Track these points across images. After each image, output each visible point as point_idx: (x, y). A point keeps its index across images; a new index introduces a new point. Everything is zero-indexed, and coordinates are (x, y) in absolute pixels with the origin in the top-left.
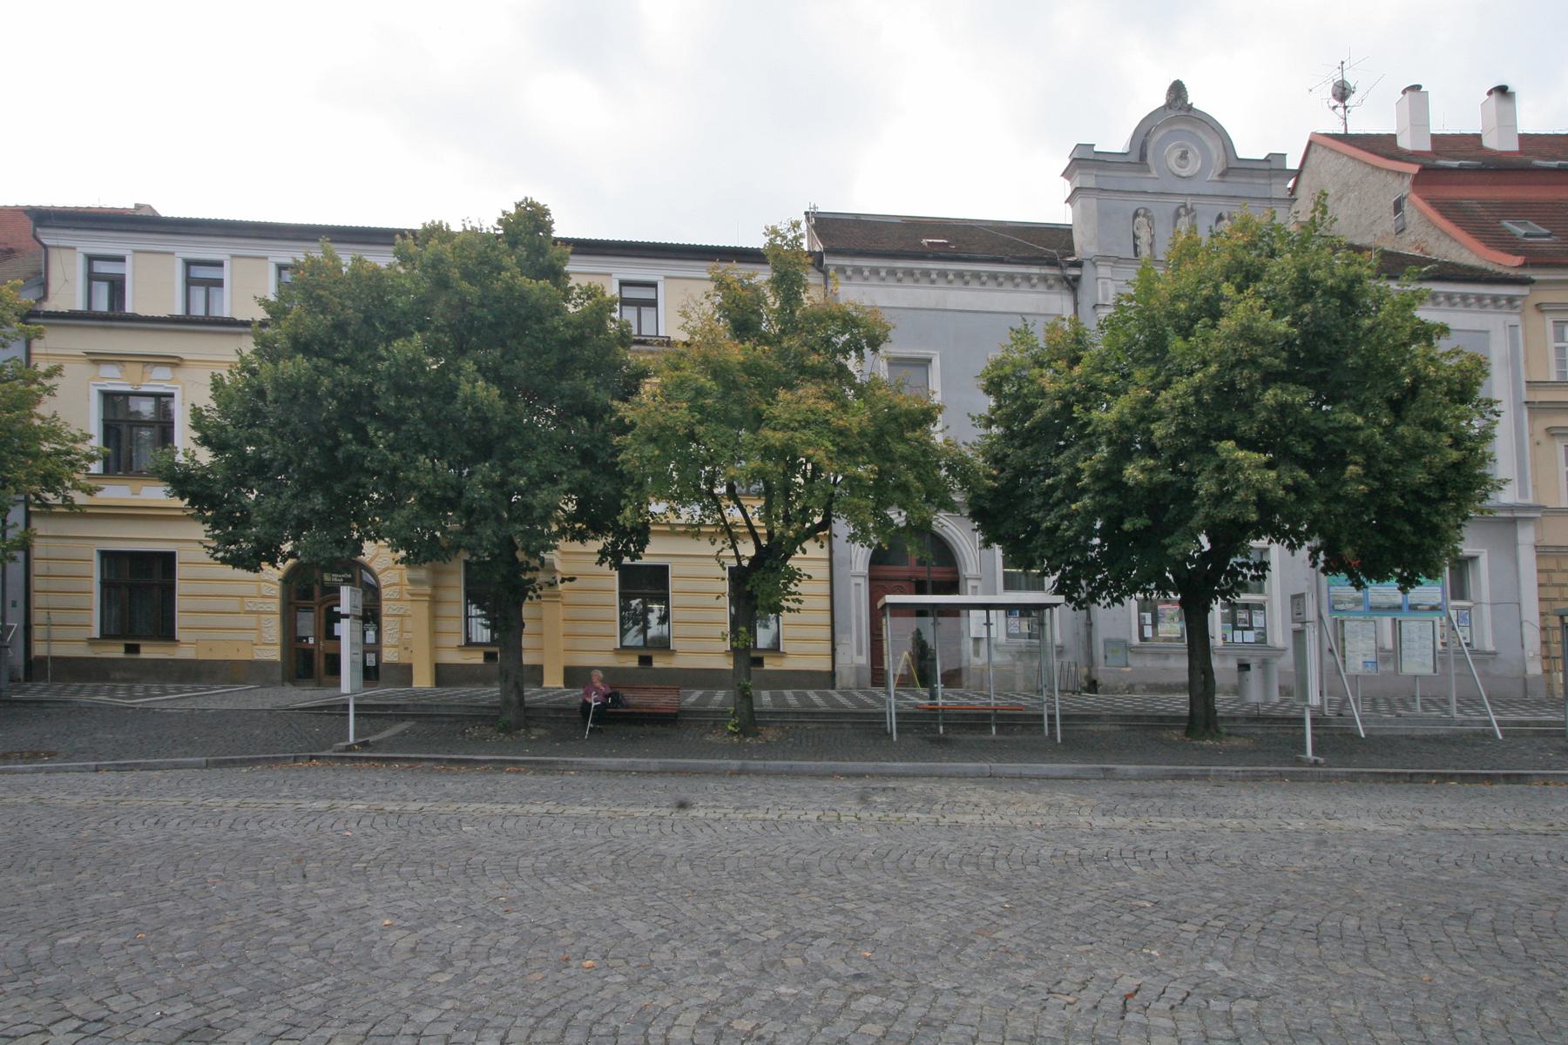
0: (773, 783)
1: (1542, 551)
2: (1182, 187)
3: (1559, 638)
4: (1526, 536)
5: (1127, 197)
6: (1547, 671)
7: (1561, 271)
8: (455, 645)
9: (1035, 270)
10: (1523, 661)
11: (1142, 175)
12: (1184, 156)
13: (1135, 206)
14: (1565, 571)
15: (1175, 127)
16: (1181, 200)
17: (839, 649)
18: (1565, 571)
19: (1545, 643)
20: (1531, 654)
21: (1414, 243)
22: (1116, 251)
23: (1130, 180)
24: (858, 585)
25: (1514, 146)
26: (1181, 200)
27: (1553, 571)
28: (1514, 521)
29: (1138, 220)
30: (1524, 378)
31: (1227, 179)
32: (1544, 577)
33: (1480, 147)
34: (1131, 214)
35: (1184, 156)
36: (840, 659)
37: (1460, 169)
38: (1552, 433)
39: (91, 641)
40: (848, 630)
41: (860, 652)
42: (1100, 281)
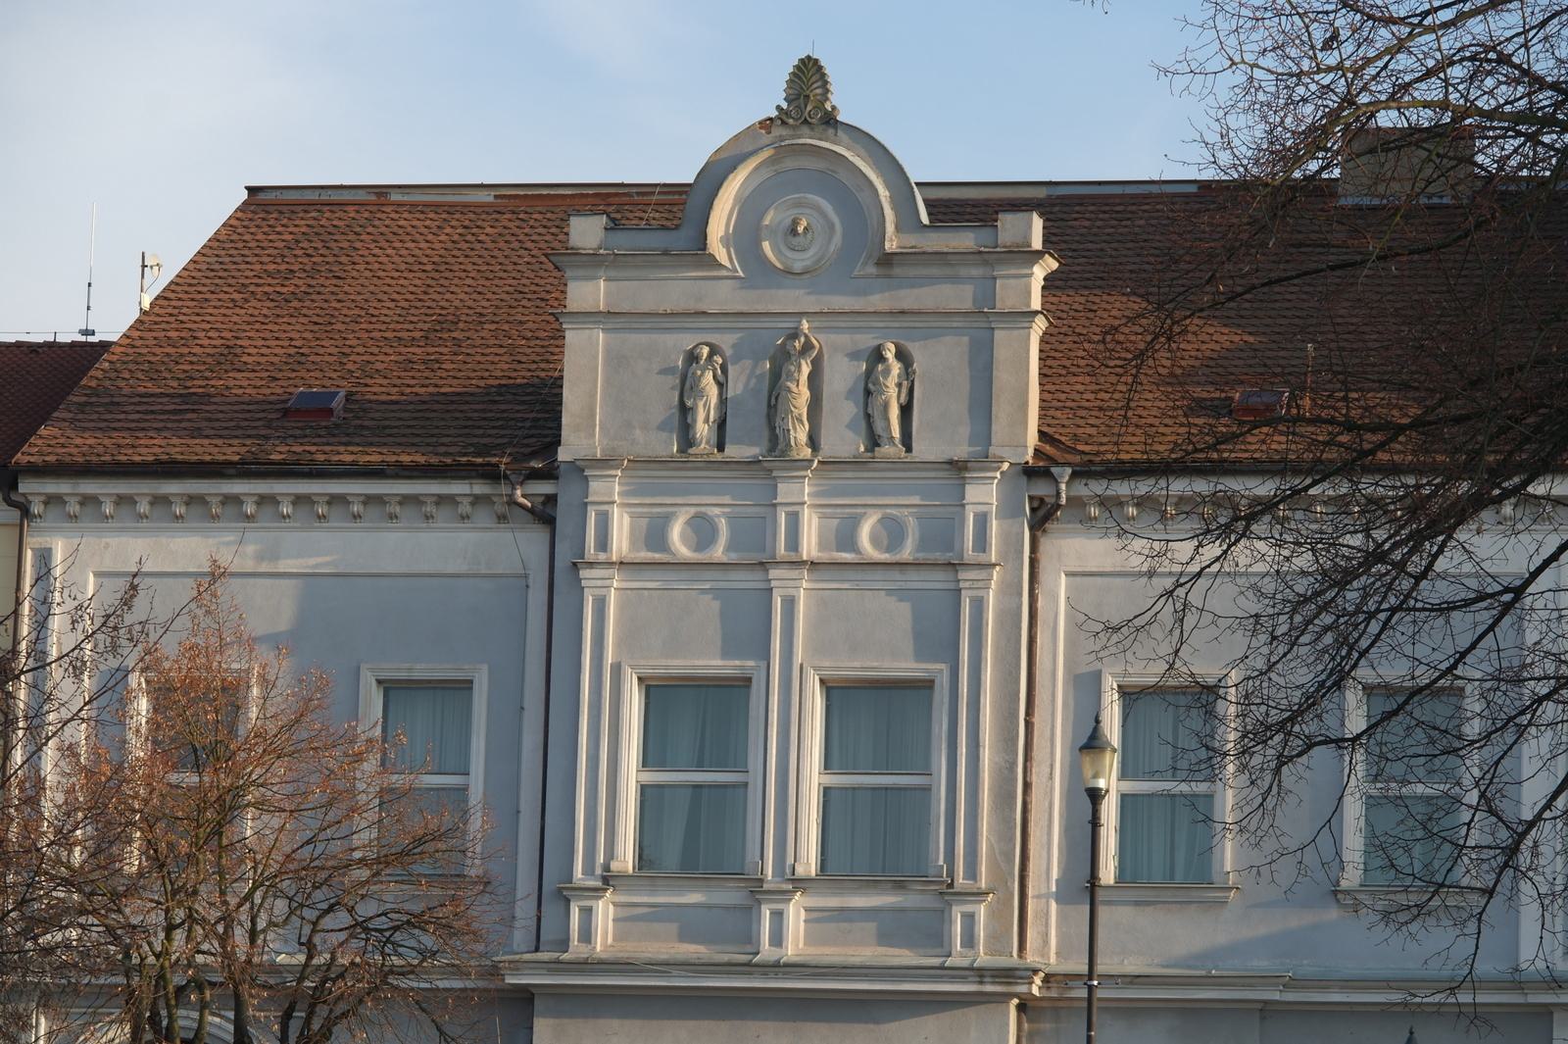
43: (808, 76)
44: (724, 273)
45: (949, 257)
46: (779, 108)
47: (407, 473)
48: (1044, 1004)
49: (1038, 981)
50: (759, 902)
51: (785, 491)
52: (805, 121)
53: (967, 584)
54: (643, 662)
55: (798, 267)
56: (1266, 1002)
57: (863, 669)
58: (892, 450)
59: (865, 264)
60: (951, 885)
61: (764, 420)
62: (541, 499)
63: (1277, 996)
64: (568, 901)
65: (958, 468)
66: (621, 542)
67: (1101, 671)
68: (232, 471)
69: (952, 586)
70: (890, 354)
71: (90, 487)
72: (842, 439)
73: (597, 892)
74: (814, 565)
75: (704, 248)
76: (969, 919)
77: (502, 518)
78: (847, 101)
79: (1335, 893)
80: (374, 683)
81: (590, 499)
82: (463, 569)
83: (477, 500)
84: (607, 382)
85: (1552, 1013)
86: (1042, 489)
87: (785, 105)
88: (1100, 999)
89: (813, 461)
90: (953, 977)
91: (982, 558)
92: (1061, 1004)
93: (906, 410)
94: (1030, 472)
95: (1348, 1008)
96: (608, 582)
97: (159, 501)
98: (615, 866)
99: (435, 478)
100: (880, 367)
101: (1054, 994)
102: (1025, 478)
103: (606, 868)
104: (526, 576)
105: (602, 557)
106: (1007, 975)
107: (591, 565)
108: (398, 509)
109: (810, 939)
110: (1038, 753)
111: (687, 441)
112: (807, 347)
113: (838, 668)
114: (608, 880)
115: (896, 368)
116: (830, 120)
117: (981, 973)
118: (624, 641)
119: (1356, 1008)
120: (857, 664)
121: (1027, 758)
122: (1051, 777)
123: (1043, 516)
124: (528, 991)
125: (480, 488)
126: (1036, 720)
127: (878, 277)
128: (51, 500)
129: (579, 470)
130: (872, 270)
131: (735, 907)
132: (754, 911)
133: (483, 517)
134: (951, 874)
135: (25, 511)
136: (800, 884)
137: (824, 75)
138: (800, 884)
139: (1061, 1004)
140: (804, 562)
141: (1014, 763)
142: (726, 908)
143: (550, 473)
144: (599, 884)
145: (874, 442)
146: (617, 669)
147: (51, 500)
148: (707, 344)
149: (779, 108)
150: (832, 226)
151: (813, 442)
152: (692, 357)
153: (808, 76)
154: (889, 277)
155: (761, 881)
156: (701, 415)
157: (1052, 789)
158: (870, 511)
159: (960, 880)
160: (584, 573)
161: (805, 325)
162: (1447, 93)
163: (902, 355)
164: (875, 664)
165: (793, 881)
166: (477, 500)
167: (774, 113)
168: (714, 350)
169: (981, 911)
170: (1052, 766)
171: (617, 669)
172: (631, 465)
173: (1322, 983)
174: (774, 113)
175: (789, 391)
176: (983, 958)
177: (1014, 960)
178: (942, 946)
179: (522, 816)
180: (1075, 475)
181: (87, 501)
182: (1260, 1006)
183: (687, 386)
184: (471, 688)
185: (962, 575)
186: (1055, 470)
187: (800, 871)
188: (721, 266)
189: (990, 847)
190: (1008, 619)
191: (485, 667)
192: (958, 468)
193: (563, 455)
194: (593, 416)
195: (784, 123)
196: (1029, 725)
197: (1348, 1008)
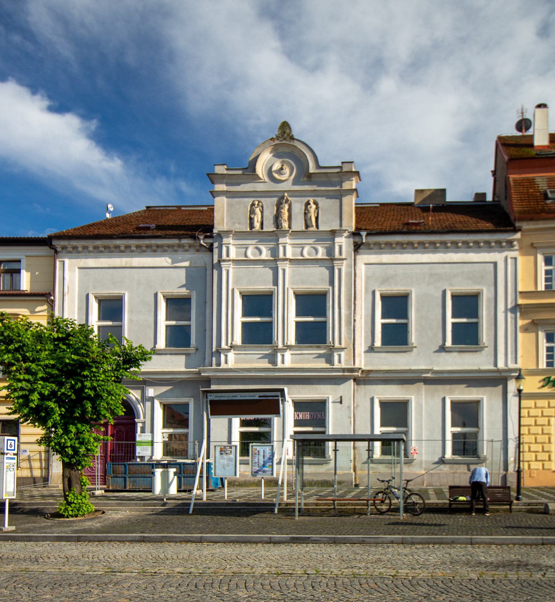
25: (145, 209)
44: (261, 181)
46: (276, 135)
48: (361, 379)
49: (360, 371)
50: (277, 353)
51: (281, 240)
54: (240, 288)
57: (306, 288)
59: (304, 178)
60: (334, 346)
62: (209, 244)
64: (220, 353)
65: (333, 233)
66: (233, 255)
68: (115, 237)
69: (331, 265)
70: (311, 202)
71: (74, 243)
72: (299, 225)
73: (228, 350)
74: (291, 260)
75: (255, 172)
76: (340, 356)
77: (198, 251)
81: (223, 243)
83: (190, 246)
84: (228, 211)
86: (357, 239)
88: (506, 364)
89: (289, 230)
91: (341, 257)
93: (317, 219)
96: (229, 266)
97: (96, 248)
98: (234, 343)
100: (309, 206)
101: (364, 376)
103: (231, 344)
105: (227, 259)
106: (352, 370)
107: (224, 261)
108: (167, 248)
109: (293, 362)
110: (357, 312)
111: (252, 226)
112: (287, 201)
113: (299, 288)
114: (232, 347)
115: (314, 206)
116: (292, 138)
117: (344, 370)
118: (236, 282)
120: (304, 287)
121: (354, 313)
122: (361, 318)
123: (357, 247)
124: (209, 378)
126: (357, 302)
128: (64, 248)
129: (220, 236)
130: (305, 179)
132: (276, 356)
133: (192, 250)
134: (334, 343)
135: (56, 252)
136: (290, 347)
137: (289, 126)
138: (290, 347)
139: (366, 379)
140: (288, 259)
141: (351, 314)
144: (229, 348)
145: (307, 226)
146: (233, 290)
147: (64, 248)
148: (257, 200)
151: (290, 227)
152: (253, 205)
155: (277, 346)
156: (256, 220)
157: (361, 321)
158: (307, 246)
159: (337, 345)
160: (222, 263)
161: (286, 194)
162: (62, 434)
163: (315, 203)
164: (309, 287)
165: (287, 346)
166: (190, 246)
167: (275, 137)
168: (259, 202)
169: (343, 354)
170: (361, 315)
171: (233, 290)
172: (235, 233)
174: (275, 137)
175: (282, 212)
176: (343, 365)
177: (352, 367)
179: (207, 331)
180: (368, 235)
181: (75, 248)
183: (252, 212)
185: (334, 262)
187: (289, 343)
188: (261, 179)
189: (345, 337)
190: (349, 274)
192: (333, 233)
193: (215, 231)
194: (223, 220)
195: (278, 139)
196: (355, 304)
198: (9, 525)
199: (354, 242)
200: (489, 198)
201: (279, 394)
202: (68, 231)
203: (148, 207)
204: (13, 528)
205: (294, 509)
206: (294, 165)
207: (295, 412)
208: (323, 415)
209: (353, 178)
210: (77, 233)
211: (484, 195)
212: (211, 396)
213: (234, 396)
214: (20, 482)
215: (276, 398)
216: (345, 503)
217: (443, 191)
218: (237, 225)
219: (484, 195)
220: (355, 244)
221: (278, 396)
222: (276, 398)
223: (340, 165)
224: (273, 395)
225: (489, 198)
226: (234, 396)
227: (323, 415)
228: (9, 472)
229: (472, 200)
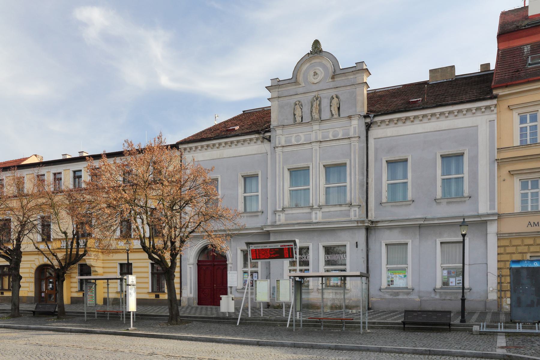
0: (34, 332)
1: (500, 237)
2: (315, 88)
3: (509, 281)
4: (492, 229)
5: (290, 98)
6: (500, 298)
7: (518, 87)
8: (115, 292)
9: (253, 136)
10: (487, 293)
11: (297, 86)
12: (315, 74)
13: (294, 101)
14: (538, 245)
15: (313, 61)
16: (314, 94)
17: (183, 291)
18: (538, 245)
19: (500, 283)
20: (491, 289)
21: (132, 170)
22: (286, 122)
23: (292, 89)
24: (190, 268)
25: (242, 112)
26: (314, 94)
27: (508, 246)
28: (485, 222)
29: (296, 106)
30: (496, 147)
31: (336, 80)
32: (502, 250)
33: (527, 17)
34: (293, 105)
35: (315, 74)
36: (183, 295)
37: (531, 27)
38: (511, 173)
39: (149, 293)
40: (186, 284)
41: (191, 293)
42: (277, 136)
43: (316, 43)
45: (346, 74)
46: (310, 51)
47: (243, 134)
52: (316, 53)
53: (352, 142)
55: (315, 82)
56: (420, 224)
58: (335, 116)
61: (310, 115)
63: (422, 223)
67: (199, 304)
68: (213, 138)
69: (349, 143)
78: (324, 47)
79: (380, 290)
80: (241, 177)
82: (256, 153)
85: (487, 222)
86: (368, 120)
87: (312, 50)
90: (352, 223)
92: (375, 228)
94: (365, 117)
95: (439, 224)
99: (248, 135)
102: (364, 119)
104: (267, 153)
116: (321, 51)
119: (441, 224)
125: (257, 136)
127: (332, 81)
131: (308, 213)
142: (306, 213)
143: (269, 131)
149: (310, 51)
150: (322, 73)
153: (316, 43)
154: (334, 81)
167: (310, 52)
173: (433, 219)
174: (310, 52)
178: (350, 217)
182: (419, 225)
184: (258, 176)
186: (370, 115)
191: (260, 171)
193: (271, 127)
195: (311, 54)
197: (439, 224)
198: (133, 326)
199: (366, 123)
200: (493, 67)
201: (292, 244)
202: (189, 138)
203: (244, 111)
204: (134, 328)
205: (360, 326)
206: (323, 72)
207: (325, 254)
208: (345, 256)
209: (364, 74)
210: (195, 138)
211: (488, 65)
212: (251, 246)
213: (265, 246)
214: (140, 302)
215: (291, 247)
216: (349, 322)
217: (453, 67)
218: (286, 121)
219: (488, 65)
220: (367, 124)
221: (292, 245)
222: (291, 247)
223: (355, 65)
224: (289, 245)
225: (493, 67)
226: (265, 246)
227: (345, 256)
228: (154, 296)
229: (480, 71)
